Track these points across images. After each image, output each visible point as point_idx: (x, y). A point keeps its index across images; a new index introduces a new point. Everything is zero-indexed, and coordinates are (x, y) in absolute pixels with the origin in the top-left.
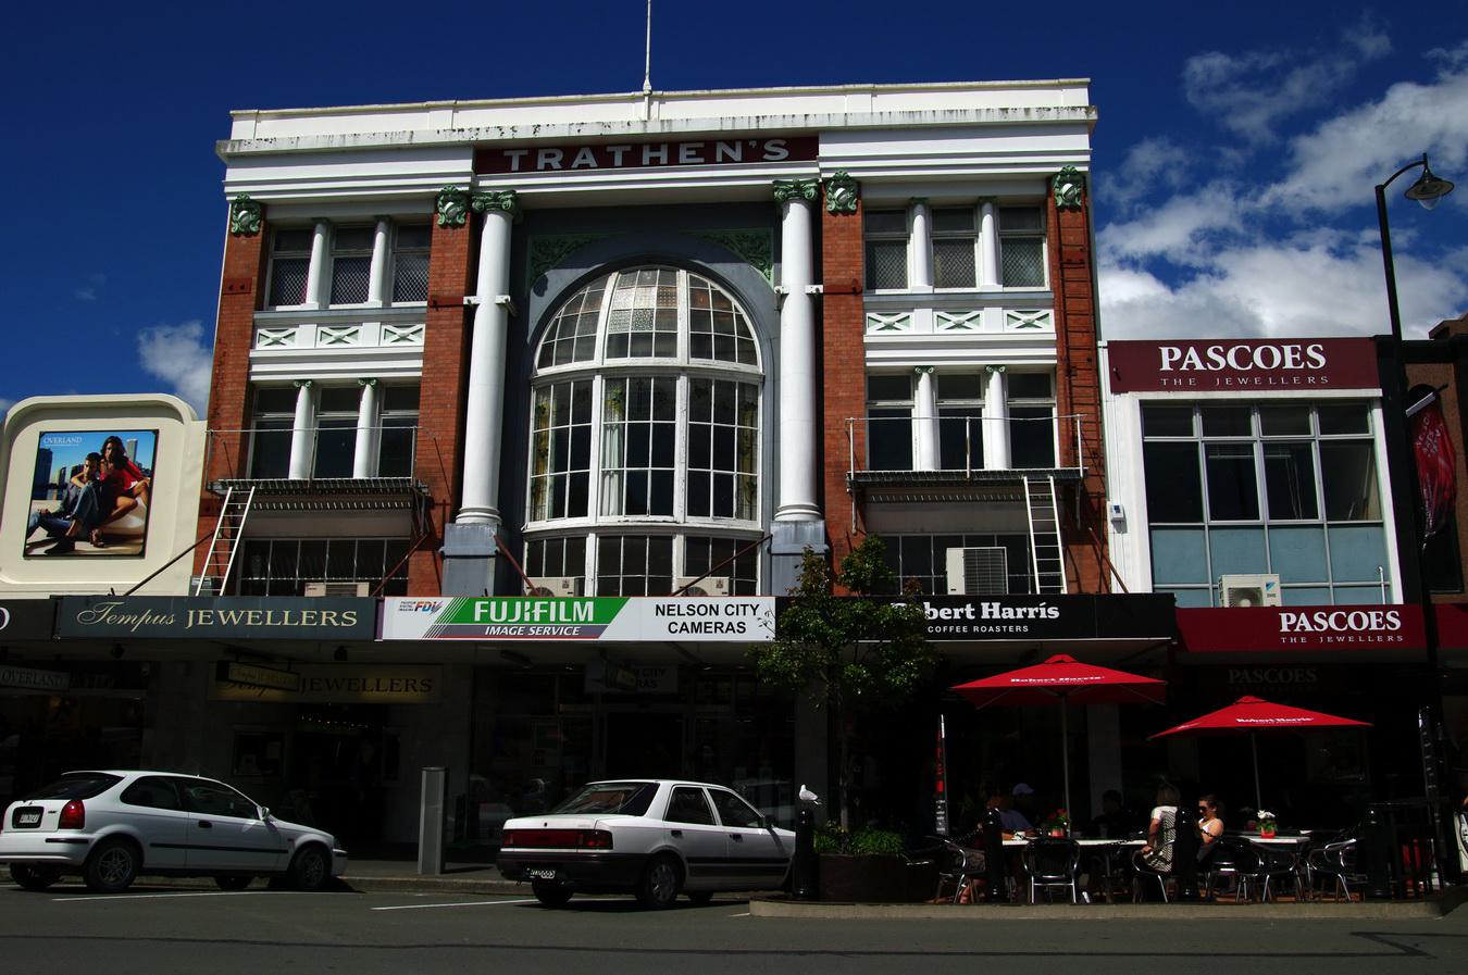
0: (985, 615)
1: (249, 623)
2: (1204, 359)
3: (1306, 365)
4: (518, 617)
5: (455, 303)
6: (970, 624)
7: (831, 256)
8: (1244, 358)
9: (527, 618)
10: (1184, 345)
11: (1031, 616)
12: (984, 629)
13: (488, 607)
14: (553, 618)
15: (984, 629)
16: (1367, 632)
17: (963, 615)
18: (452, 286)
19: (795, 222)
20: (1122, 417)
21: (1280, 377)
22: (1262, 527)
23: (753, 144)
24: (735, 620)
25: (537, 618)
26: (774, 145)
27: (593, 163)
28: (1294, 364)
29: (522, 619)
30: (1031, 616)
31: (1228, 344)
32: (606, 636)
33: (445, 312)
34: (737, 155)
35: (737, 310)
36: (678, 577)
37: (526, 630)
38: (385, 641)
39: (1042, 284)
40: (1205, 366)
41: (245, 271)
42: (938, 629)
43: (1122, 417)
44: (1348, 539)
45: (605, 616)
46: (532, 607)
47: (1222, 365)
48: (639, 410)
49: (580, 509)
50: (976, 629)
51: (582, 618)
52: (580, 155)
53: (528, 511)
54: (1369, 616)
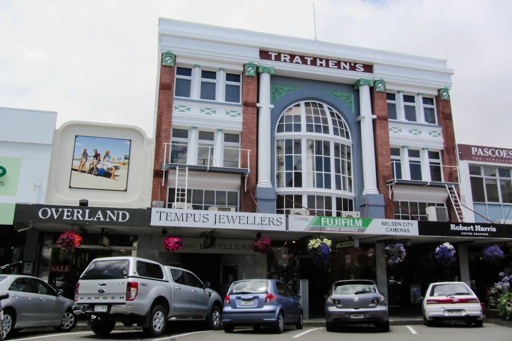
0: (476, 230)
1: (65, 218)
4: (337, 223)
6: (473, 232)
7: (377, 106)
8: (493, 153)
9: (340, 225)
10: (478, 147)
11: (489, 230)
12: (476, 234)
13: (326, 220)
14: (348, 225)
15: (476, 234)
17: (471, 229)
18: (252, 99)
20: (463, 168)
21: (502, 159)
22: (501, 205)
23: (353, 64)
24: (406, 228)
25: (343, 225)
27: (301, 62)
29: (338, 225)
30: (489, 230)
31: (489, 148)
32: (366, 233)
33: (250, 108)
34: (348, 67)
36: (334, 210)
37: (340, 229)
38: (290, 232)
39: (239, 102)
41: (169, 81)
42: (464, 233)
43: (463, 168)
44: (179, 188)
45: (366, 224)
46: (341, 221)
47: (488, 155)
48: (319, 152)
49: (299, 183)
50: (474, 234)
51: (358, 225)
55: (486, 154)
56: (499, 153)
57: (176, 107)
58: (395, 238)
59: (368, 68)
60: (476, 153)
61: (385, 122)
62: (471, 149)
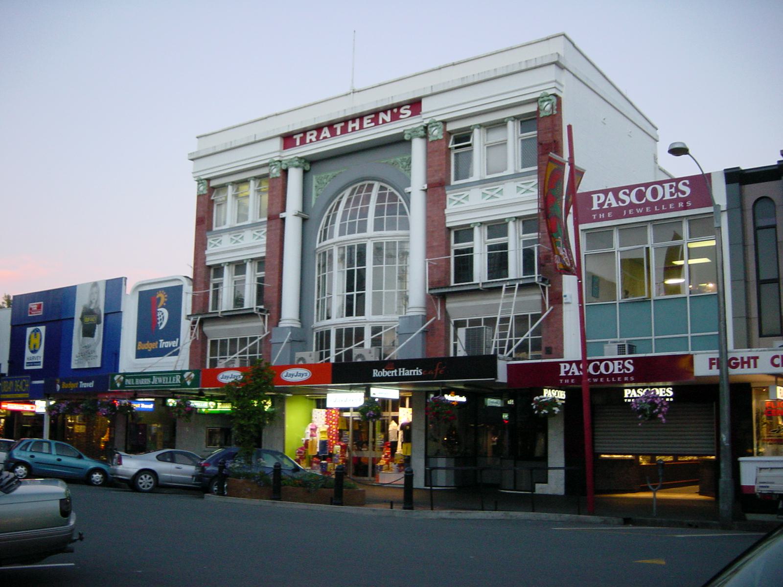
2: (617, 199)
3: (678, 195)
5: (277, 217)
10: (605, 192)
16: (612, 375)
19: (418, 147)
21: (663, 205)
26: (405, 109)
28: (671, 196)
31: (631, 188)
35: (400, 201)
40: (618, 204)
48: (351, 263)
52: (323, 132)
53: (315, 317)
54: (613, 363)
55: (623, 201)
56: (607, 367)
57: (210, 243)
58: (471, 169)
59: (415, 105)
60: (567, 372)
61: (440, 189)
62: (560, 366)
